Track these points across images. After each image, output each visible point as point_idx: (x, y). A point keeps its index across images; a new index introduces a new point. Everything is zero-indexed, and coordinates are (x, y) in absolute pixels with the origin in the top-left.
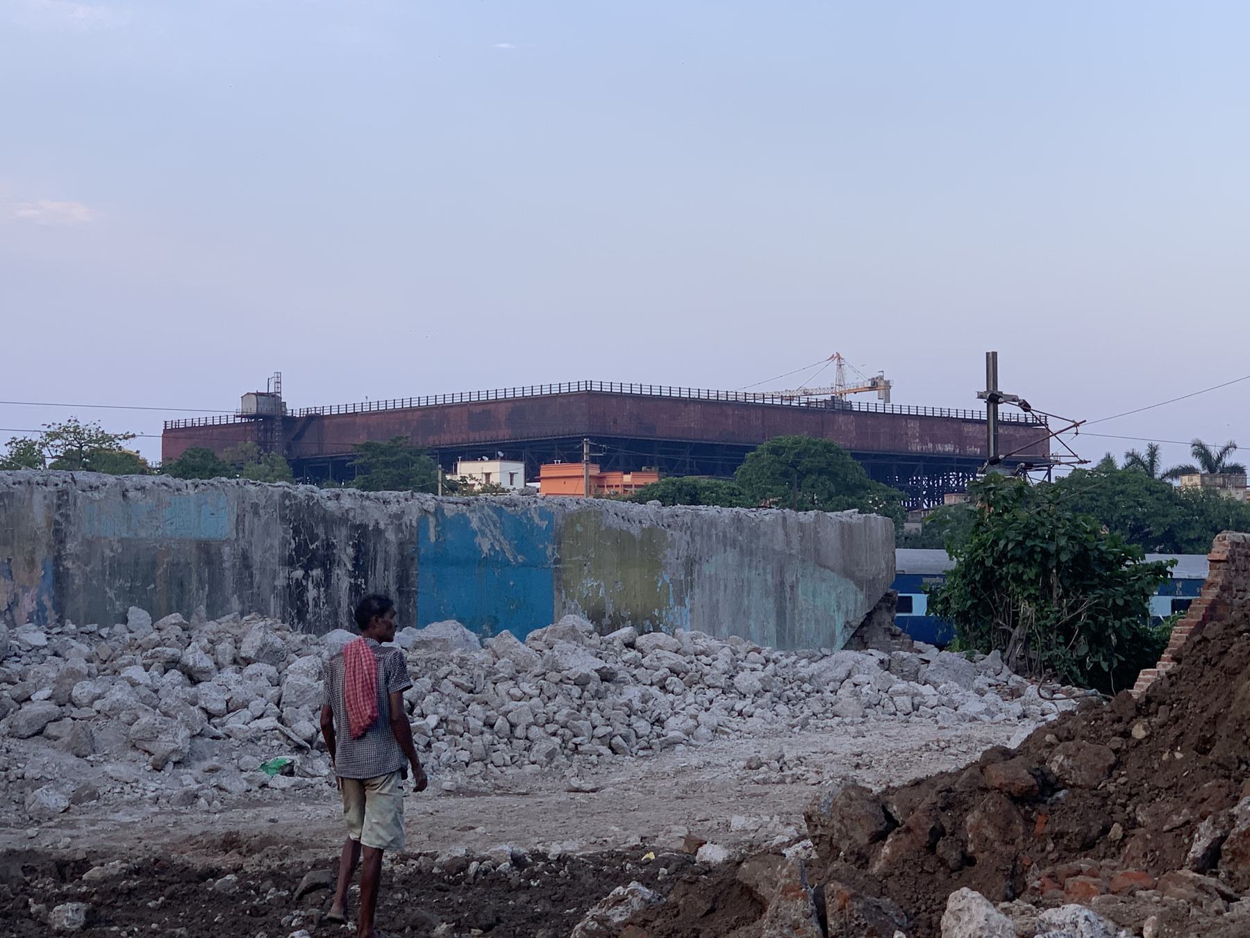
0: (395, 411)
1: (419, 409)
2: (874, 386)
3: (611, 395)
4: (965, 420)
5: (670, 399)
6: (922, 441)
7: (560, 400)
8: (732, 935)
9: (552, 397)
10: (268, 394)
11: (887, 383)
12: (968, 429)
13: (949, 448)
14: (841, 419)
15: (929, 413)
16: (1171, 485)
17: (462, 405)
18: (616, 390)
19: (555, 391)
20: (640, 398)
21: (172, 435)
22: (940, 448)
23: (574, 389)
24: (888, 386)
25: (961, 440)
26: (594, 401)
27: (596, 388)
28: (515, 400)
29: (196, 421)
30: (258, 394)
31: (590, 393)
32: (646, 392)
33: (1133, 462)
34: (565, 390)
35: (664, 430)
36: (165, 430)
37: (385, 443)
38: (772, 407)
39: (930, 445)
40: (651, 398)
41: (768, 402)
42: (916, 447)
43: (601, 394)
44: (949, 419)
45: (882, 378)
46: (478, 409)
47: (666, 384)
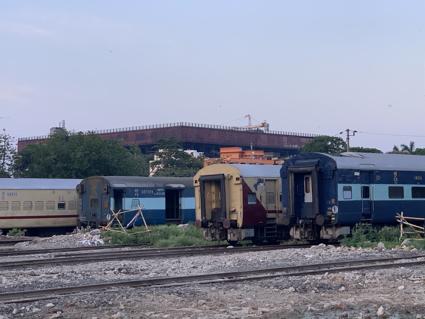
0: (107, 134)
1: (117, 133)
2: (263, 125)
3: (189, 127)
4: (303, 137)
5: (208, 129)
6: (288, 144)
7: (171, 129)
8: (183, 318)
9: (168, 128)
10: (60, 128)
11: (268, 124)
12: (303, 140)
13: (296, 146)
14: (262, 136)
15: (290, 134)
16: (335, 163)
17: (133, 131)
18: (191, 125)
19: (169, 126)
20: (198, 128)
21: (21, 143)
22: (293, 146)
23: (176, 125)
24: (268, 126)
25: (300, 143)
26: (183, 129)
27: (184, 125)
28: (153, 129)
29: (228, 127)
30: (56, 128)
31: (182, 127)
32: (200, 126)
33: (405, 149)
34: (173, 126)
35: (206, 140)
36: (19, 141)
37: (167, 140)
38: (241, 132)
39: (290, 145)
40: (202, 128)
41: (242, 130)
42: (286, 146)
43: (186, 127)
44: (296, 136)
45: (265, 123)
46: (139, 133)
47: (128, 127)
